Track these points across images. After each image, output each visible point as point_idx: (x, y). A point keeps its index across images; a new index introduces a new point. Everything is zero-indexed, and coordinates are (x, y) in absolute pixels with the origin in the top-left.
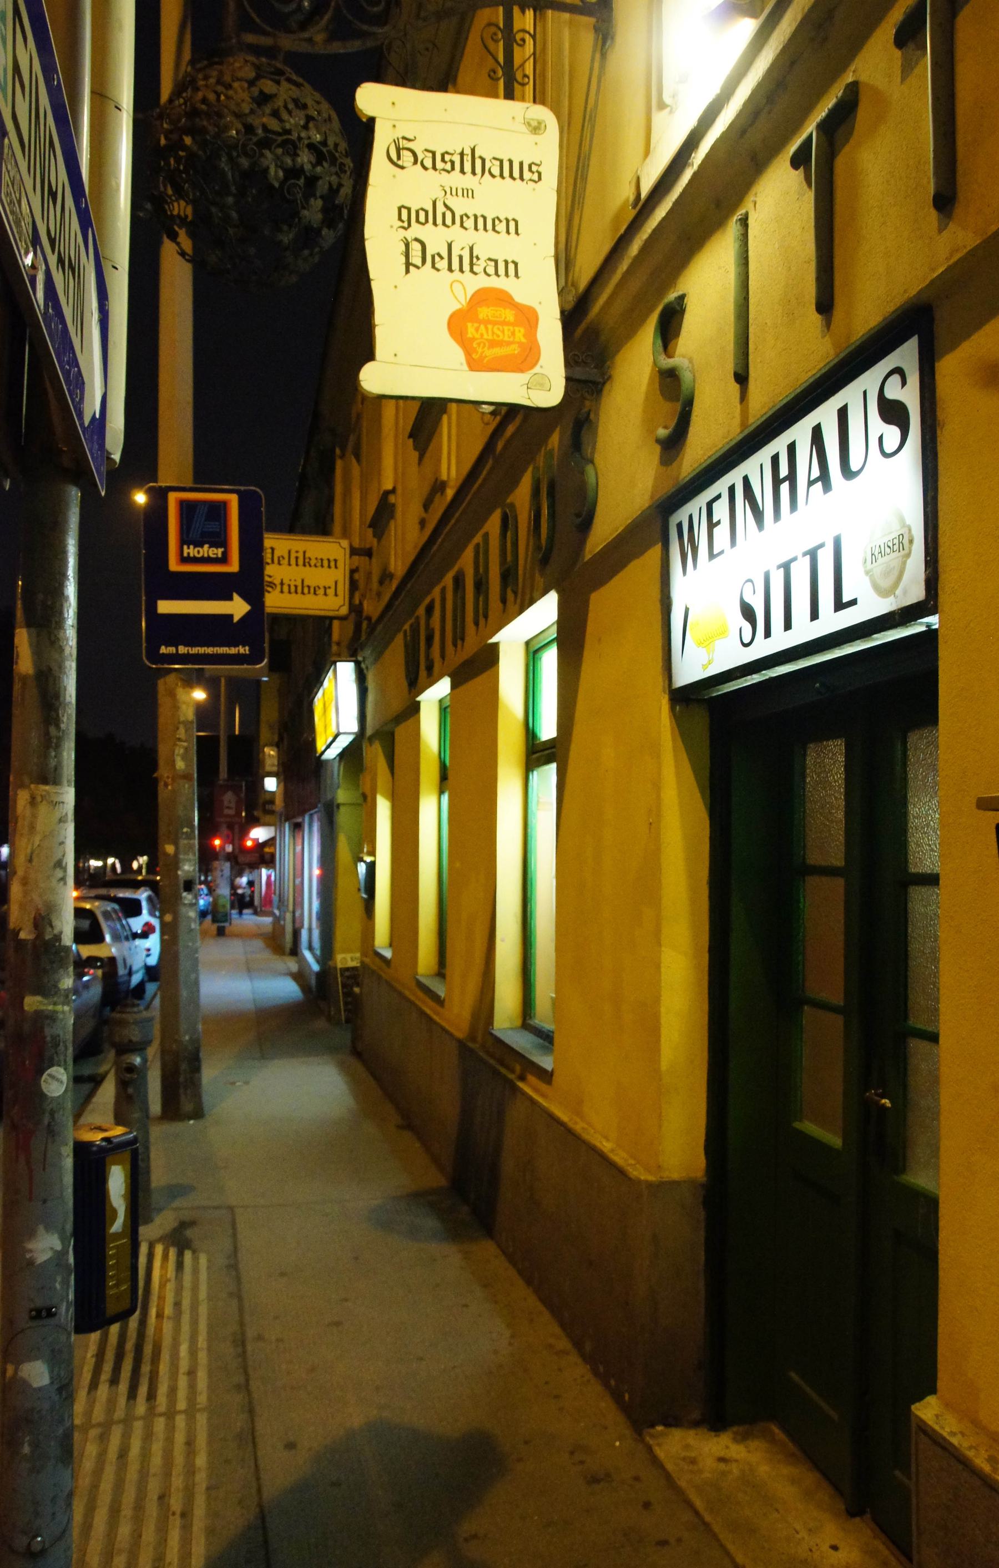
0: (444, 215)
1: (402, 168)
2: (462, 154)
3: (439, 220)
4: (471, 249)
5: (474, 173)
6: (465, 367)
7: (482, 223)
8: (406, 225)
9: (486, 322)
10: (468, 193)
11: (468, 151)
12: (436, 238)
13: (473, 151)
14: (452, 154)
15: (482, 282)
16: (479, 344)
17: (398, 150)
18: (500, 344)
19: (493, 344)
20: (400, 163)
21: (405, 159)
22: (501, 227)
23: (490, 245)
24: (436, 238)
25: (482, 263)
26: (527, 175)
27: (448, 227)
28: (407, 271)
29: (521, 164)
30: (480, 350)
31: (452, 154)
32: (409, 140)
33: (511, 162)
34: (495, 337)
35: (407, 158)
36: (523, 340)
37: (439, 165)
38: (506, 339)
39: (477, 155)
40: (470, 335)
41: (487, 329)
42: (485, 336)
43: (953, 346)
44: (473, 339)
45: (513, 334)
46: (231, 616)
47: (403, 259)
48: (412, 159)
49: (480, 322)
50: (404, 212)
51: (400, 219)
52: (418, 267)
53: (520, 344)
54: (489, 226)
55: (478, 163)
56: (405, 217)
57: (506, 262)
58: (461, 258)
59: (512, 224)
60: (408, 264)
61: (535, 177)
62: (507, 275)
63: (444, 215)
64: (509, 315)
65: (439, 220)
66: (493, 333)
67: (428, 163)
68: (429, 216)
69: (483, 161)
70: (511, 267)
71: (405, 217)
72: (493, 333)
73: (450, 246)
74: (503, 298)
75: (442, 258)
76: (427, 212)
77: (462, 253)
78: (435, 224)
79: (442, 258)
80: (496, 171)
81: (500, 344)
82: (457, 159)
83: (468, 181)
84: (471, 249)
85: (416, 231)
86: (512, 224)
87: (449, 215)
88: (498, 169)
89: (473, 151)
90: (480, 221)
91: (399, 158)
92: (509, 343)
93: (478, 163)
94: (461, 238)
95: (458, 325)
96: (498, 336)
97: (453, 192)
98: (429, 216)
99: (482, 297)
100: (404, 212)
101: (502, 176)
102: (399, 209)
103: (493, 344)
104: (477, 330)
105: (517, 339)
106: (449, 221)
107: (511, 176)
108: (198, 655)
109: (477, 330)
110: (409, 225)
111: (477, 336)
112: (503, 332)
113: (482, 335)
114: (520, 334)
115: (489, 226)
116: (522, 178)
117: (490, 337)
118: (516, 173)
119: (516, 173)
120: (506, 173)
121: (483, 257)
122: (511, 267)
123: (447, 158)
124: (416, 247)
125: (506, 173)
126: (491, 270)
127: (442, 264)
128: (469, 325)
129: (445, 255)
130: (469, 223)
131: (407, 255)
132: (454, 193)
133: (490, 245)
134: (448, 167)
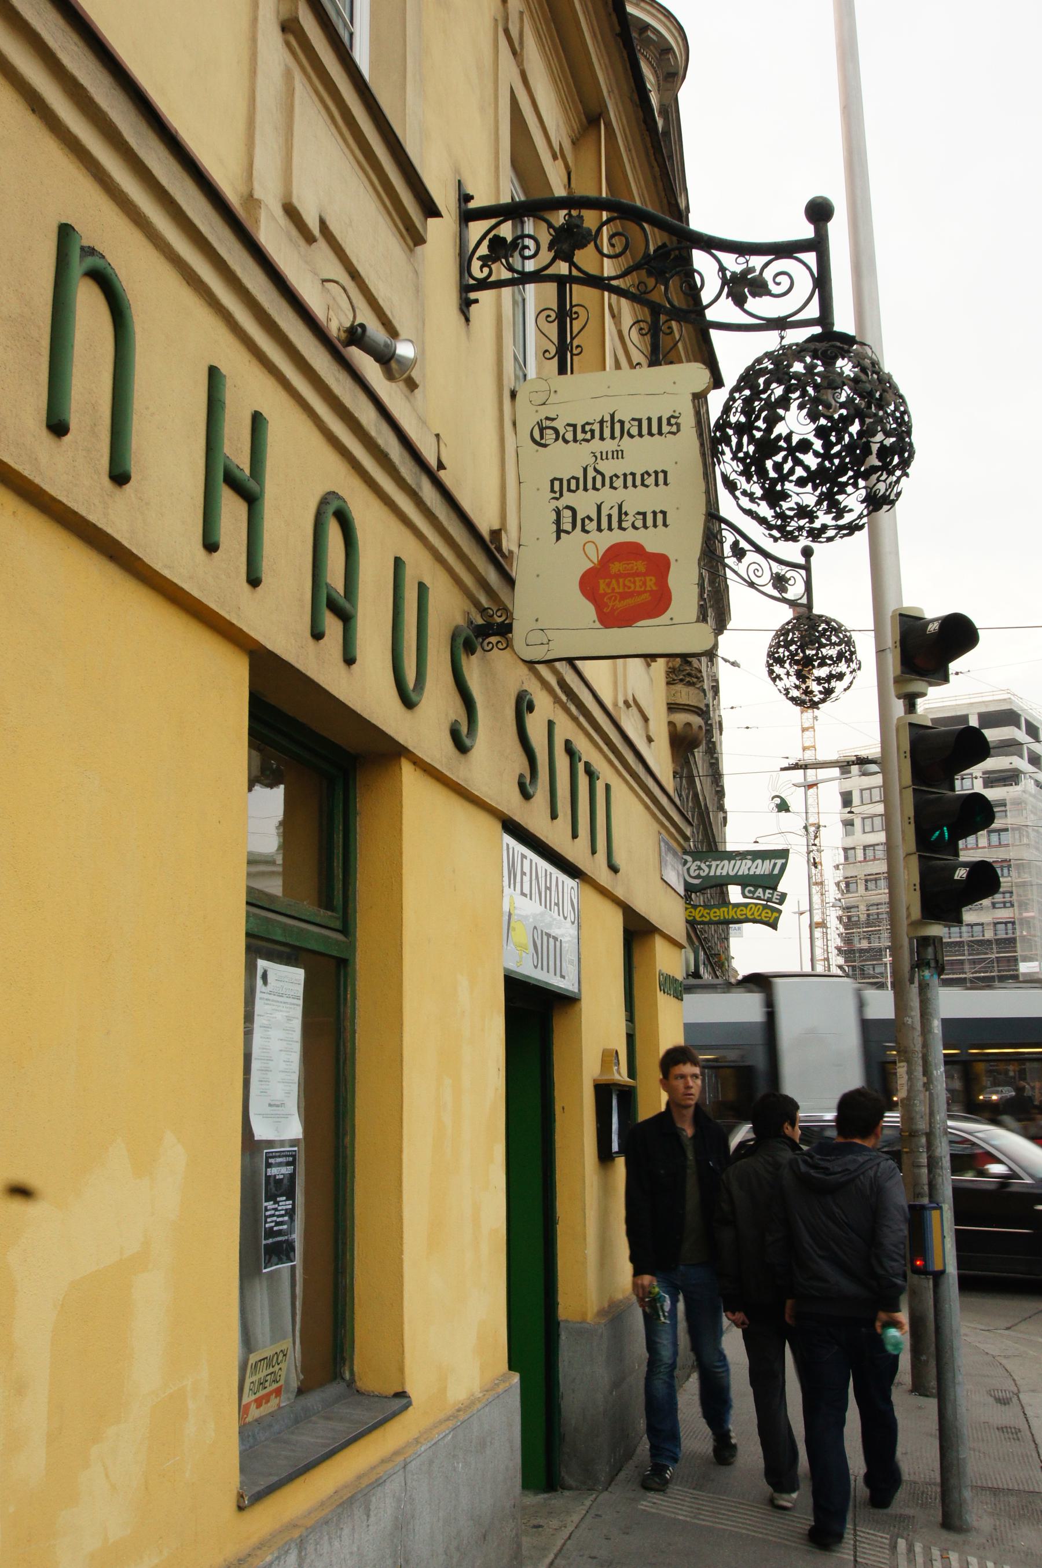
0: (594, 479)
1: (545, 446)
2: (602, 422)
3: (590, 485)
4: (620, 507)
5: (613, 437)
6: (598, 625)
7: (631, 480)
8: (557, 495)
9: (618, 576)
10: (618, 454)
11: (607, 418)
12: (584, 503)
13: (612, 416)
14: (669, 433)
15: (618, 537)
16: (610, 598)
17: (542, 430)
18: (631, 595)
19: (623, 596)
20: (543, 442)
21: (548, 437)
22: (650, 481)
23: (636, 500)
24: (584, 503)
25: (630, 518)
26: (665, 428)
27: (598, 490)
28: (558, 538)
29: (660, 419)
30: (611, 604)
31: (669, 433)
32: (553, 419)
33: (649, 419)
34: (627, 590)
35: (550, 435)
36: (654, 588)
37: (580, 436)
38: (638, 589)
39: (616, 420)
40: (601, 591)
41: (618, 583)
42: (617, 590)
43: (258, 228)
44: (606, 594)
45: (644, 584)
46: (965, 718)
47: (554, 527)
48: (554, 436)
49: (611, 577)
50: (557, 484)
51: (553, 491)
52: (568, 533)
53: (651, 592)
54: (638, 482)
55: (617, 426)
56: (557, 487)
57: (655, 513)
58: (610, 516)
59: (661, 476)
60: (559, 532)
61: (674, 429)
62: (655, 526)
63: (594, 479)
64: (640, 566)
65: (590, 485)
66: (624, 585)
67: (569, 436)
68: (580, 483)
69: (622, 423)
70: (660, 517)
71: (557, 487)
72: (624, 585)
73: (599, 507)
74: (634, 550)
75: (591, 520)
76: (577, 479)
77: (611, 512)
78: (586, 489)
79: (591, 520)
80: (634, 431)
81: (631, 595)
82: (596, 427)
83: (609, 445)
84: (620, 507)
85: (568, 499)
86: (661, 476)
87: (599, 478)
88: (636, 428)
89: (612, 416)
90: (630, 478)
91: (542, 438)
92: (639, 593)
93: (617, 426)
94: (609, 498)
95: (589, 584)
96: (629, 588)
97: (604, 456)
98: (580, 483)
99: (616, 552)
100: (557, 484)
101: (640, 435)
102: (552, 482)
103: (623, 596)
104: (608, 585)
105: (648, 589)
106: (599, 485)
107: (650, 434)
108: (647, 795)
109: (608, 585)
110: (561, 495)
111: (609, 591)
112: (634, 582)
113: (613, 589)
114: (651, 582)
115: (638, 482)
116: (660, 433)
117: (621, 590)
118: (655, 430)
119: (655, 430)
120: (645, 431)
121: (631, 513)
122: (660, 517)
123: (587, 428)
124: (567, 513)
125: (645, 431)
126: (639, 523)
127: (592, 526)
128: (601, 581)
129: (594, 516)
130: (619, 483)
131: (558, 522)
132: (604, 457)
133: (636, 500)
134: (588, 436)
